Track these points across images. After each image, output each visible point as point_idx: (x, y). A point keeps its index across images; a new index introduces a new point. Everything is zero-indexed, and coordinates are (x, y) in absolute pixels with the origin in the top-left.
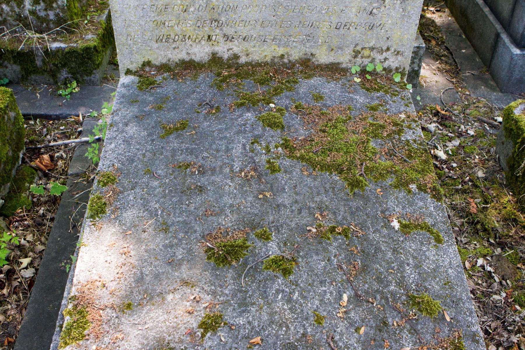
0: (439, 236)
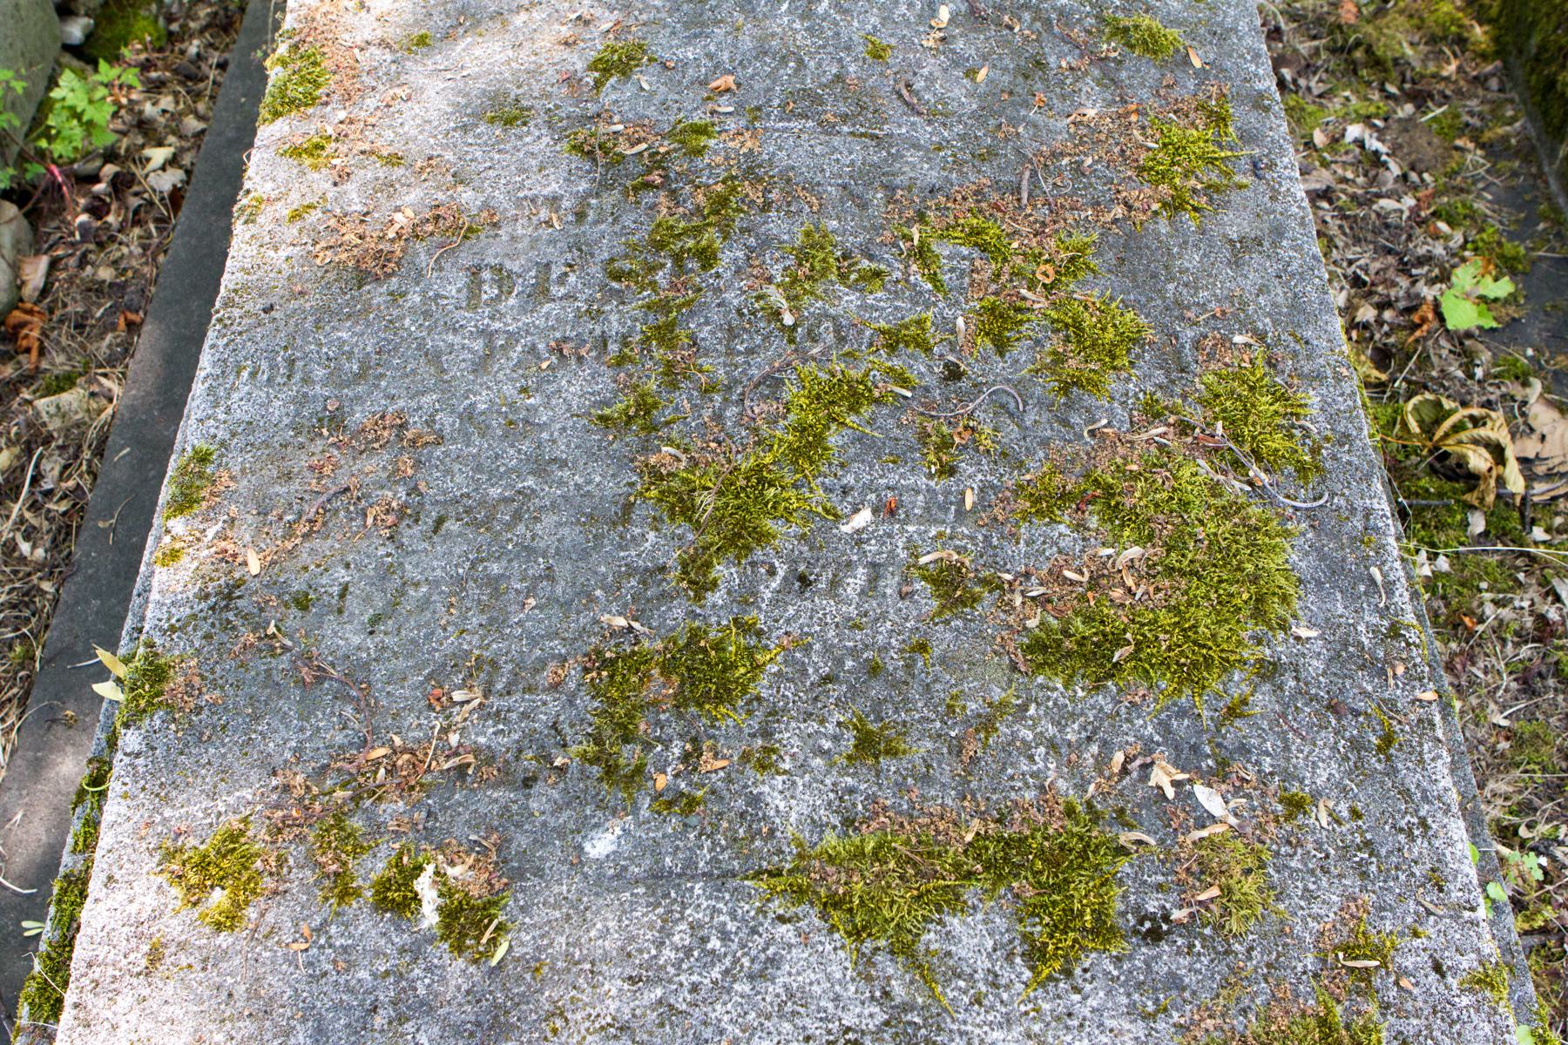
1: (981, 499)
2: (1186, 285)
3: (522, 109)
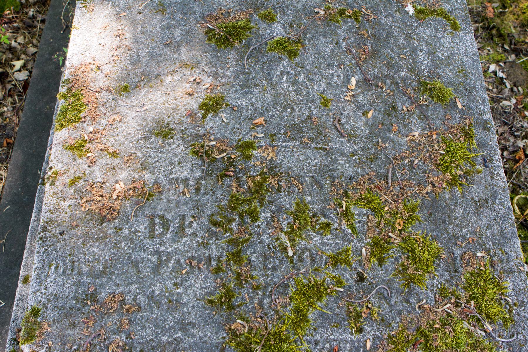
0: (455, 23)
1: (373, 343)
2: (457, 226)
3: (170, 130)
